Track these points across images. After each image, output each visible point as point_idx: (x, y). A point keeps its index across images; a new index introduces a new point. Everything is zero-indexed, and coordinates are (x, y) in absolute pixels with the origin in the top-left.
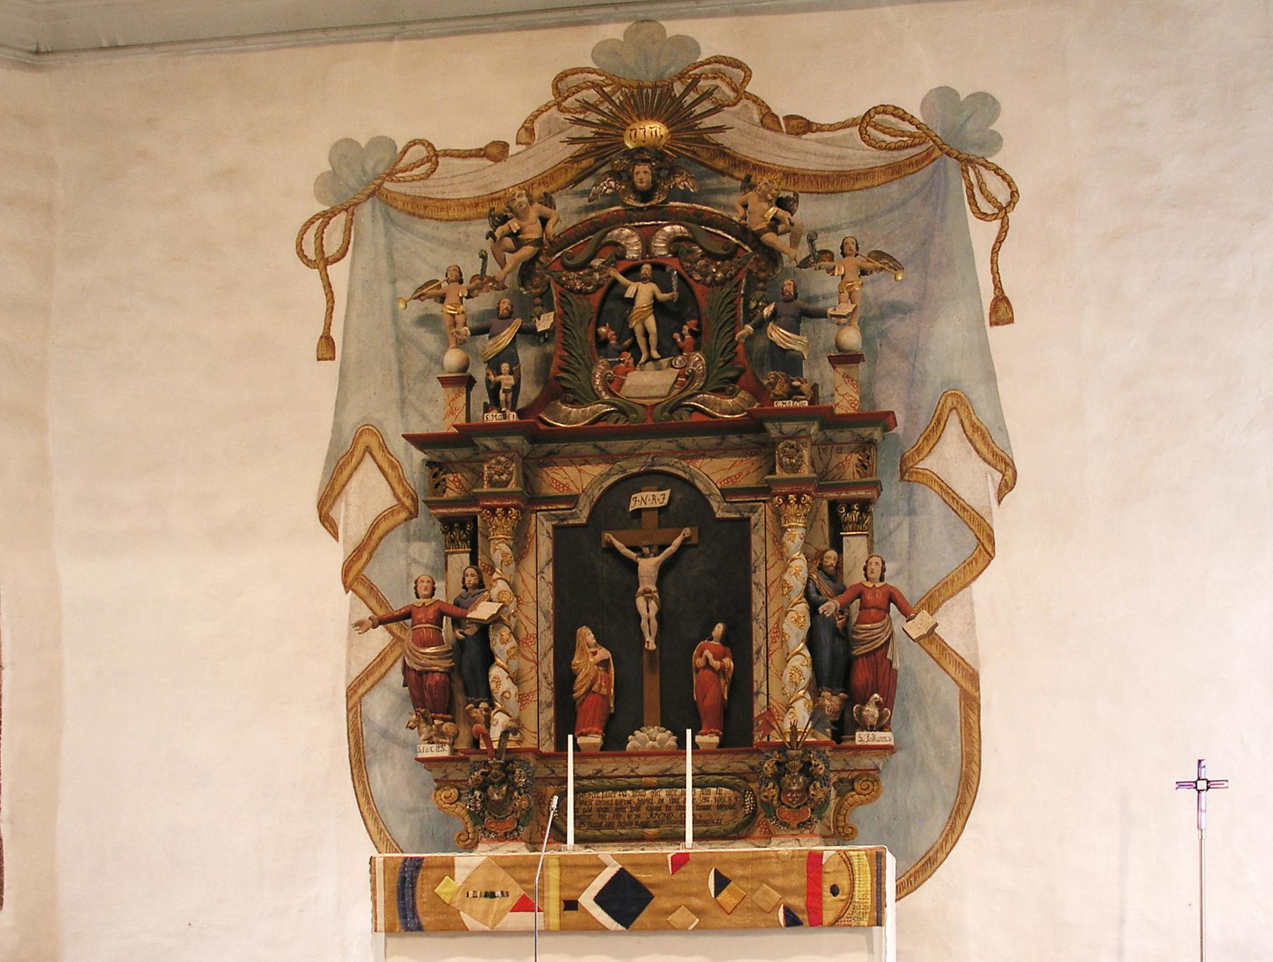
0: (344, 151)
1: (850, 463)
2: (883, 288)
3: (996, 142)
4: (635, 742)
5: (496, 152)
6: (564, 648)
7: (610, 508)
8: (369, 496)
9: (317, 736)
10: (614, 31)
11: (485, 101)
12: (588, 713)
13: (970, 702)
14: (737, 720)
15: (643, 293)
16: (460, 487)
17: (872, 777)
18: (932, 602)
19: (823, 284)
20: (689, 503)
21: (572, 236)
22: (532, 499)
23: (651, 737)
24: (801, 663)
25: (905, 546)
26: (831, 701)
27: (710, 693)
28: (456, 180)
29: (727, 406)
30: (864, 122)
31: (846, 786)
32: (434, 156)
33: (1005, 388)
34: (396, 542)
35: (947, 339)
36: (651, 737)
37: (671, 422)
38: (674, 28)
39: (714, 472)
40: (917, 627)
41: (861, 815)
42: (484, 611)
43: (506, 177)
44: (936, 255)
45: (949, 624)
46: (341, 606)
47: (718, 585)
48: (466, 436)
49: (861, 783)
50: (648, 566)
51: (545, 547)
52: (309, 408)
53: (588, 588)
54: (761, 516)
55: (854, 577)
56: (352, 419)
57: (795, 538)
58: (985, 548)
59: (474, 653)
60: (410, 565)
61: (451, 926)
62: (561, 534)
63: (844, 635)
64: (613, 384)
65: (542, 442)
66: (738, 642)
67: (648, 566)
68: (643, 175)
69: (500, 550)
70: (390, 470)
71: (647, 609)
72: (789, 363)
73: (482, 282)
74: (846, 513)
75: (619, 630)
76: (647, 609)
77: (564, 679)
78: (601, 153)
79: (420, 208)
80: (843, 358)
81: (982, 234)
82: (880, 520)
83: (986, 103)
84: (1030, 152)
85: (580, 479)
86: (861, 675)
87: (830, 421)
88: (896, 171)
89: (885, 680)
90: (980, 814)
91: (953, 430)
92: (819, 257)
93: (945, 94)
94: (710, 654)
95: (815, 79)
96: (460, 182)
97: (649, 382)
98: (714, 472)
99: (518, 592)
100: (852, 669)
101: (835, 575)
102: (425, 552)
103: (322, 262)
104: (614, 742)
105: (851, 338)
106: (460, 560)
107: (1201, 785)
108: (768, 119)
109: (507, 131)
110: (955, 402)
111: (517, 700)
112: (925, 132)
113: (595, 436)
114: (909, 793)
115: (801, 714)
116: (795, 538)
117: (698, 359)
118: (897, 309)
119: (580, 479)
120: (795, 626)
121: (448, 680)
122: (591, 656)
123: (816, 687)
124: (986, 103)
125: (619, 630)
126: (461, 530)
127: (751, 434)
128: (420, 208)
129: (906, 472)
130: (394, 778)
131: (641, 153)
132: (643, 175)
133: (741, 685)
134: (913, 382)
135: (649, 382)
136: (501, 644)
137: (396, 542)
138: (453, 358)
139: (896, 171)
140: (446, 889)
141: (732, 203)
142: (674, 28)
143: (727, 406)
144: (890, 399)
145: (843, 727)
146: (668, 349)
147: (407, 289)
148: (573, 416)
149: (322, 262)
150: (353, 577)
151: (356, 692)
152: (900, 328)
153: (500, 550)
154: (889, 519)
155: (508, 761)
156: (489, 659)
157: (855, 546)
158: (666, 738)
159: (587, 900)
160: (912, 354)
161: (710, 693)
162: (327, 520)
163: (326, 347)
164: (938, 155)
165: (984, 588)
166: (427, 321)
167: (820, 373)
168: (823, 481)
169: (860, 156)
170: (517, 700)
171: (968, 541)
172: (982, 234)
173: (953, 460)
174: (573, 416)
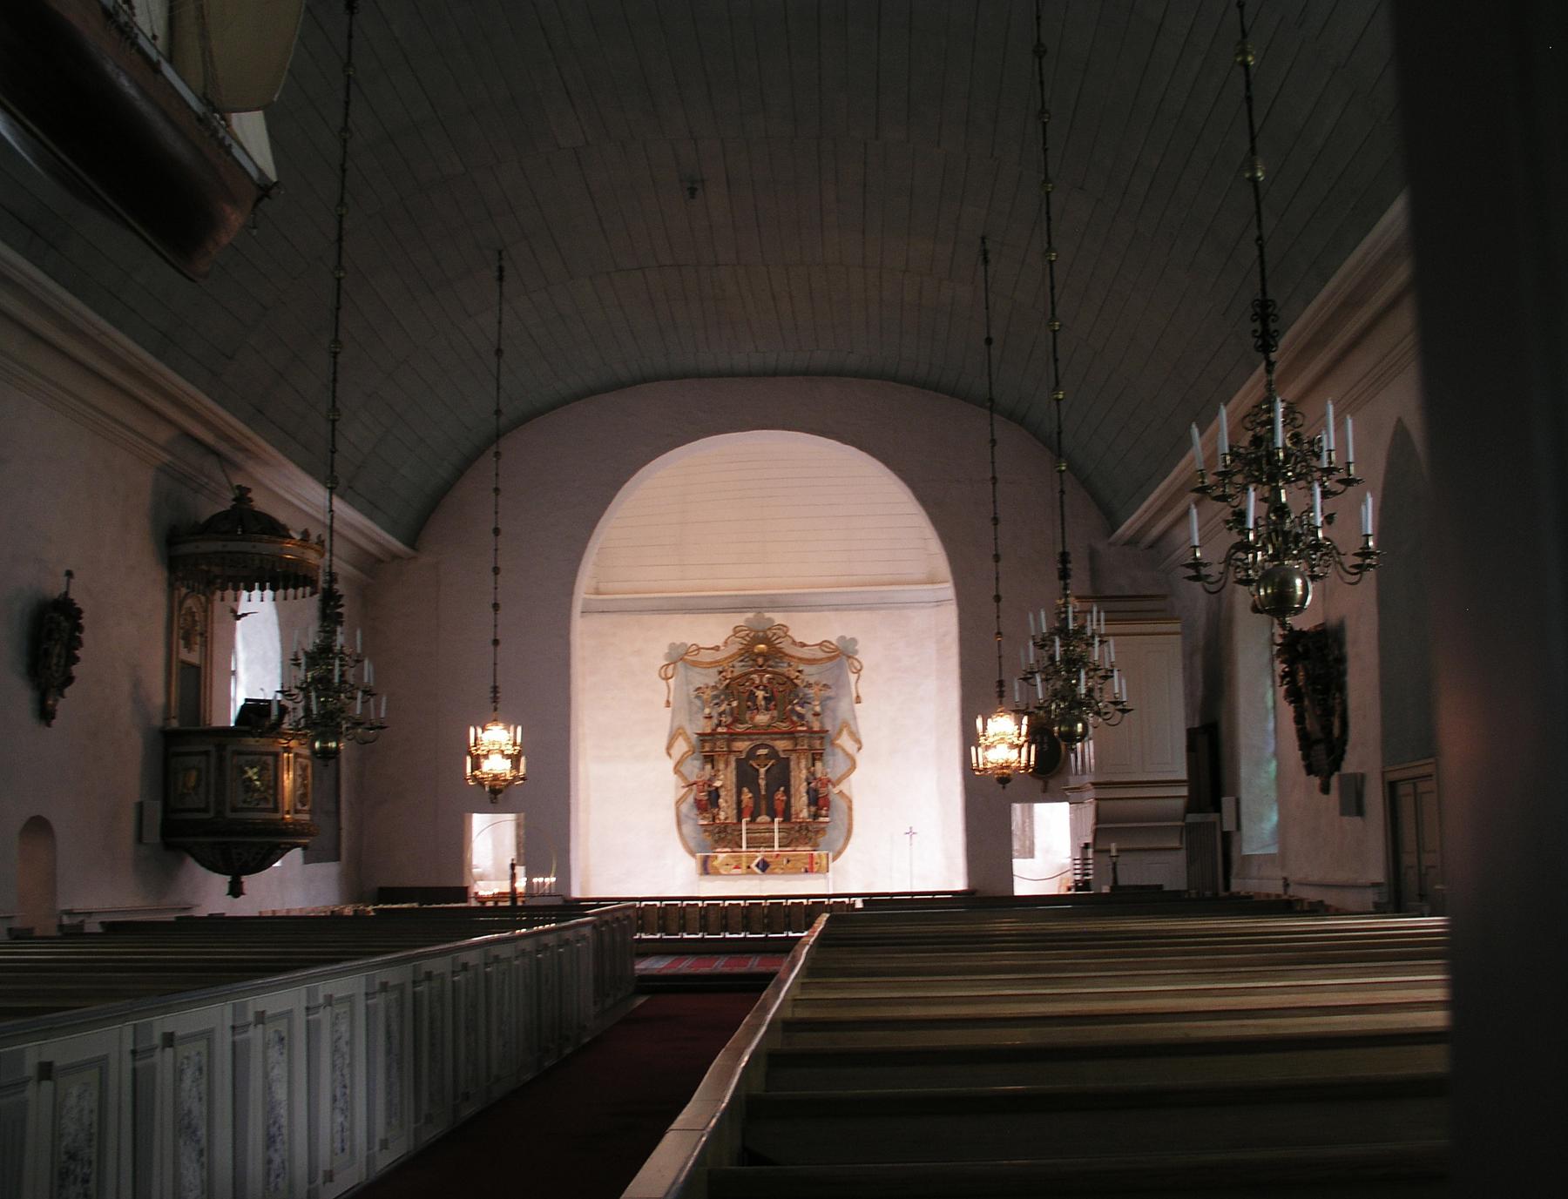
0: (672, 646)
1: (817, 743)
2: (828, 693)
3: (856, 652)
4: (759, 819)
5: (717, 648)
6: (739, 793)
7: (751, 753)
8: (681, 747)
9: (666, 817)
10: (750, 615)
11: (713, 634)
12: (747, 811)
13: (850, 809)
14: (787, 816)
15: (760, 694)
16: (709, 748)
17: (823, 829)
18: (839, 781)
19: (811, 692)
20: (774, 754)
21: (740, 676)
22: (730, 752)
23: (764, 818)
24: (805, 799)
25: (830, 767)
26: (813, 809)
27: (780, 807)
28: (346, 1071)
29: (784, 726)
30: (820, 645)
31: (817, 832)
32: (699, 649)
33: (859, 721)
34: (689, 761)
35: (843, 706)
36: (764, 818)
37: (767, 731)
38: (767, 615)
39: (781, 745)
40: (836, 791)
41: (821, 840)
42: (718, 784)
43: (719, 656)
44: (840, 683)
45: (843, 787)
46: (673, 778)
47: (781, 776)
48: (713, 734)
49: (820, 831)
50: (762, 770)
51: (733, 764)
52: (663, 720)
53: (745, 777)
54: (793, 757)
55: (819, 775)
56: (676, 724)
57: (803, 764)
58: (853, 766)
59: (714, 795)
60: (694, 769)
61: (717, 873)
62: (738, 761)
63: (816, 791)
64: (752, 719)
65: (733, 737)
66: (787, 792)
67: (762, 770)
68: (760, 661)
69: (722, 766)
70: (687, 739)
71: (762, 783)
72: (801, 716)
73: (715, 687)
74: (816, 756)
75: (755, 788)
76: (762, 783)
77: (739, 802)
78: (747, 653)
79: (695, 664)
80: (817, 714)
81: (853, 677)
82: (825, 757)
83: (854, 641)
84: (868, 654)
85: (743, 746)
86: (821, 802)
87: (811, 731)
88: (830, 659)
89: (827, 804)
90: (852, 840)
91: (845, 733)
92: (809, 685)
93: (842, 638)
94: (780, 796)
95: (809, 631)
96: (706, 657)
97: (762, 718)
98: (781, 745)
99: (726, 779)
100: (818, 801)
101: (813, 774)
102: (697, 763)
103: (667, 679)
104: (753, 821)
105: (818, 709)
106: (709, 767)
107: (911, 833)
108: (794, 642)
109: (720, 643)
110: (846, 725)
111: (726, 811)
112: (837, 649)
113: (746, 735)
114: (834, 834)
115: (805, 814)
116: (803, 764)
117: (775, 713)
118: (829, 698)
119: (743, 746)
120: (803, 788)
121: (708, 801)
122: (747, 796)
123: (809, 805)
124: (854, 641)
125: (755, 788)
126: (709, 759)
127: (791, 735)
128: (695, 664)
129: (832, 744)
130: (688, 828)
131: (760, 654)
132: (760, 661)
133: (788, 804)
134: (835, 719)
135: (762, 718)
136: (722, 793)
137: (689, 761)
138: (707, 711)
139: (830, 659)
140: (716, 863)
141: (783, 668)
142: (767, 615)
143: (784, 726)
144: (829, 727)
145: (816, 816)
146: (767, 709)
147: (692, 688)
148: (740, 728)
149: (667, 679)
150: (677, 770)
151: (678, 803)
152: (830, 703)
153: (722, 766)
154: (828, 758)
155: (726, 825)
156: (718, 797)
157: (819, 764)
158: (768, 819)
159: (753, 866)
160: (834, 711)
161: (780, 807)
162: (669, 755)
163: (668, 704)
164: (840, 655)
165: (854, 777)
166: (697, 697)
167: (809, 717)
168: (811, 748)
169: (821, 655)
170: (726, 811)
171: (849, 763)
172: (853, 677)
173: (845, 741)
174: (740, 728)
